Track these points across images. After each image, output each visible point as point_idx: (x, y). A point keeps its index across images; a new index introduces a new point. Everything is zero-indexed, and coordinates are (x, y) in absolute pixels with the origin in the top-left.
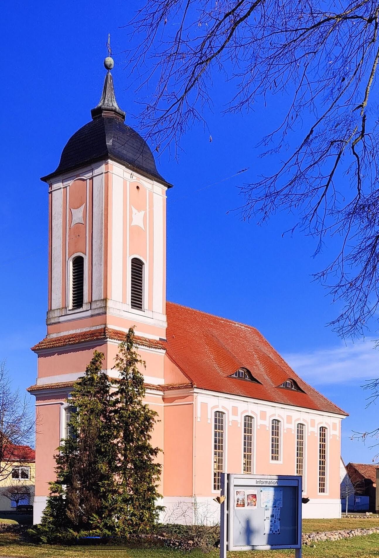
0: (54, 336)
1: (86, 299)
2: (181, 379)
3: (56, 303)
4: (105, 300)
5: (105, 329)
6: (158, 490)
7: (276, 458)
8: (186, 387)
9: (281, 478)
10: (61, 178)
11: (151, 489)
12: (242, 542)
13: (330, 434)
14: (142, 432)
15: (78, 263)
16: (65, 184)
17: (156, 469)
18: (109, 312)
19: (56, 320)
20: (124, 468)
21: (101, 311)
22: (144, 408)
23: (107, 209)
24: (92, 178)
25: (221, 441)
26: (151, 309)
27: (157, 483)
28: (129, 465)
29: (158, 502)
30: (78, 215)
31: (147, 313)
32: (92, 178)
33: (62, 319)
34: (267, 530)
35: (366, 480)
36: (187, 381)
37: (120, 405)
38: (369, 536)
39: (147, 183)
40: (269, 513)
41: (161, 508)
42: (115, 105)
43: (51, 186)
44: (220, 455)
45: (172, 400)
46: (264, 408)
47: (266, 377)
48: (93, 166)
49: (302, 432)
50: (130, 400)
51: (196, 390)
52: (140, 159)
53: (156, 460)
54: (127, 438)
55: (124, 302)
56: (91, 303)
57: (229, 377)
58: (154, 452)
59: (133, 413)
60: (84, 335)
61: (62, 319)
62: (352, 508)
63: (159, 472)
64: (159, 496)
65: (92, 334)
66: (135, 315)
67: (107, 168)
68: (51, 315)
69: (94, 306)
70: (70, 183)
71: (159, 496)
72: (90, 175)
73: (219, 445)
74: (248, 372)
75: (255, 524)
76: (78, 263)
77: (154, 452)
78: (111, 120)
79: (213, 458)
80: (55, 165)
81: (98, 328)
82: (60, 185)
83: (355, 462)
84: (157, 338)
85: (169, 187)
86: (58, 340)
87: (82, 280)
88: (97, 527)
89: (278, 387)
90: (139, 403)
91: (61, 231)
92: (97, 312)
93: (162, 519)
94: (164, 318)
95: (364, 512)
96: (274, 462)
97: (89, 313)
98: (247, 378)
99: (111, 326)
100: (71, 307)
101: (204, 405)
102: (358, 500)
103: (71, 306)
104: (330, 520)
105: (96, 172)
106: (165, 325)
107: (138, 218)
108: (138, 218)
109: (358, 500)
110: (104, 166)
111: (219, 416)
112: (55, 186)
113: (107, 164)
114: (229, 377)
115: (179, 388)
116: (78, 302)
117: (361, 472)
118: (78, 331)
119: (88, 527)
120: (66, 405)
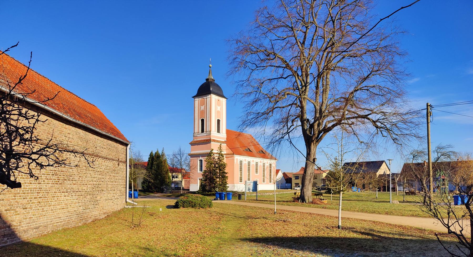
0: (196, 140)
1: (205, 130)
2: (231, 152)
3: (196, 131)
4: (210, 131)
5: (210, 139)
6: (227, 183)
7: (257, 173)
8: (232, 154)
9: (254, 181)
10: (197, 97)
11: (226, 182)
12: (248, 190)
13: (273, 165)
14: (224, 168)
15: (203, 121)
16: (199, 99)
17: (227, 177)
18: (212, 135)
19: (196, 136)
20: (219, 178)
21: (209, 134)
22: (224, 163)
23: (211, 107)
24: (206, 98)
25: (242, 169)
26: (222, 133)
27: (227, 181)
28: (220, 177)
29: (227, 185)
30: (202, 108)
31: (221, 134)
32: (206, 98)
33: (198, 135)
34: (252, 189)
35: (289, 178)
36: (232, 153)
37: (218, 162)
38: (280, 194)
39: (221, 99)
40: (252, 187)
41: (228, 187)
42: (212, 77)
43: (194, 99)
44: (241, 172)
45: (228, 158)
46: (253, 159)
47: (254, 150)
48: (207, 95)
49: (264, 165)
50: (220, 161)
51: (235, 155)
52: (219, 92)
53: (227, 175)
54: (220, 170)
55: (215, 131)
56: (206, 132)
57: (244, 151)
58: (227, 173)
59: (222, 164)
60: (204, 140)
61: (198, 135)
62: (282, 188)
63: (228, 178)
64: (227, 184)
65: (207, 140)
66: (218, 135)
67: (211, 96)
68: (195, 134)
69: (207, 133)
70: (200, 99)
71: (227, 184)
72: (206, 97)
73: (241, 170)
74: (249, 149)
75: (250, 188)
76: (203, 121)
77: (227, 173)
78: (211, 82)
79: (239, 173)
80: (195, 93)
81: (209, 138)
82: (197, 99)
83: (286, 172)
84: (224, 141)
85: (227, 99)
86: (197, 141)
87: (204, 124)
88: (213, 191)
89: (257, 153)
90: (223, 162)
91: (197, 112)
92: (208, 134)
93: (229, 189)
94: (226, 135)
95: (288, 189)
96: (256, 174)
97: (206, 134)
98: (249, 151)
99: (212, 138)
100: (200, 132)
101: (237, 159)
102: (286, 185)
103: (200, 132)
104: (271, 190)
105: (208, 97)
106: (226, 137)
107: (219, 108)
108: (219, 108)
109: (286, 185)
110: (210, 96)
111: (241, 162)
112: (196, 99)
113: (211, 95)
114: (244, 151)
115: (230, 154)
116: (203, 131)
117: (288, 175)
118: (203, 139)
119: (211, 191)
120: (199, 159)
